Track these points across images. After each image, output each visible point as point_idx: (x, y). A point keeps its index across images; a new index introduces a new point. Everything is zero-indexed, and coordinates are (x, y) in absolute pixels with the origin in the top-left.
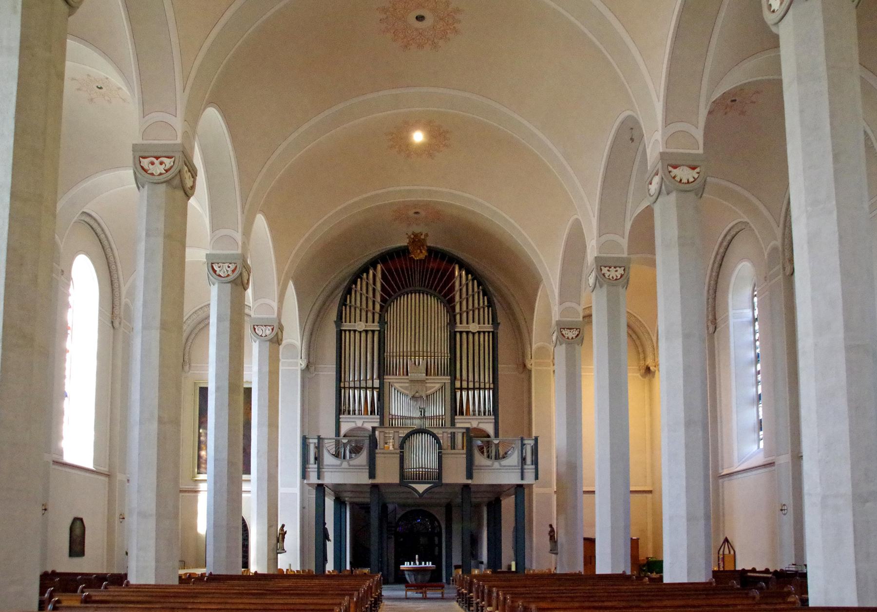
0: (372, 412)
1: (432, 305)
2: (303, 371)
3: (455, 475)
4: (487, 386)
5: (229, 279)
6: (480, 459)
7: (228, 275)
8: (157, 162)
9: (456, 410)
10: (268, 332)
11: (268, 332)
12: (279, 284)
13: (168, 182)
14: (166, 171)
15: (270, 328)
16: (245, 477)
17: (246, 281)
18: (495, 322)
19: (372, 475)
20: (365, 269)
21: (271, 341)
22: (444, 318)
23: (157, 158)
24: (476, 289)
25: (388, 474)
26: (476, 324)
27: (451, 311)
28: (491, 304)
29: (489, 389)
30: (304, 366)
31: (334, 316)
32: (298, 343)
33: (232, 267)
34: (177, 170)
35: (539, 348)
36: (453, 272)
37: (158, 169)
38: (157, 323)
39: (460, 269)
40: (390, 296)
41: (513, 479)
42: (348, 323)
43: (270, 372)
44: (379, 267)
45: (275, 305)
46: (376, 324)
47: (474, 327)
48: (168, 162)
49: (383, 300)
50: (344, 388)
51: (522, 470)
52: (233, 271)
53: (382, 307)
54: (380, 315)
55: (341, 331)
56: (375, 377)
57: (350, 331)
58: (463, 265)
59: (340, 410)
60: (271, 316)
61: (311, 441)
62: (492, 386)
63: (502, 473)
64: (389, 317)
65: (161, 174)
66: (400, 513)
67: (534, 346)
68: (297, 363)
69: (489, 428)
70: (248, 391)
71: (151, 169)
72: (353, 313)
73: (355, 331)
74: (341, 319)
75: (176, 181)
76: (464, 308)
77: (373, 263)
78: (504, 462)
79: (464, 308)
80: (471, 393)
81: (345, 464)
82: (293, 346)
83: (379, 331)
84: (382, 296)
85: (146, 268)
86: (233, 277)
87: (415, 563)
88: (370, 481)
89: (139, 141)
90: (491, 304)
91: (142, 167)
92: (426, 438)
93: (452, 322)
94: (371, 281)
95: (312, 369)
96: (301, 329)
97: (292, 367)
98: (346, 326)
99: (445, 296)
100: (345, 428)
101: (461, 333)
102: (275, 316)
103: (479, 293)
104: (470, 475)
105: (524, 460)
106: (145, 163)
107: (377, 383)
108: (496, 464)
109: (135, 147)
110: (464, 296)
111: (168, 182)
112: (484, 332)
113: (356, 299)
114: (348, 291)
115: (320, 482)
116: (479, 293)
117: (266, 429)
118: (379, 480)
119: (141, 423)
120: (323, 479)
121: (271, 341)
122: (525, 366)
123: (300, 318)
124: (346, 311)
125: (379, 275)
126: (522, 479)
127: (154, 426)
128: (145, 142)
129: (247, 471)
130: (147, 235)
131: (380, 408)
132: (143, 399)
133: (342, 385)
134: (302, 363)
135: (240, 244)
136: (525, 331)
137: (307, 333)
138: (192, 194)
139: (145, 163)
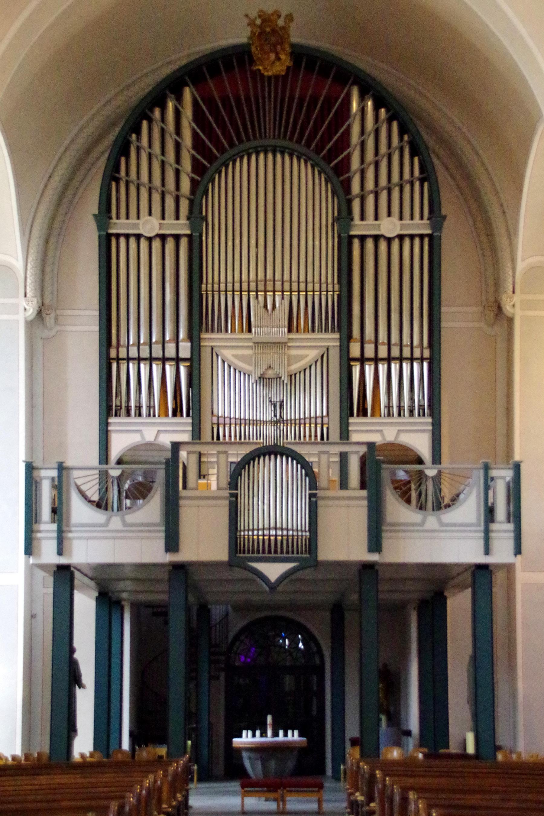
2: (30, 325)
3: (344, 541)
4: (417, 353)
9: (353, 404)
18: (435, 215)
19: (172, 543)
20: (156, 99)
22: (327, 207)
25: (205, 542)
28: (427, 175)
29: (422, 359)
30: (31, 312)
31: (92, 205)
32: (18, 264)
35: (532, 268)
40: (211, 158)
42: (123, 221)
44: (187, 94)
46: (183, 221)
47: (389, 227)
51: (487, 532)
53: (194, 184)
54: (192, 203)
55: (109, 236)
58: (369, 88)
59: (109, 408)
61: (44, 473)
62: (427, 354)
63: (440, 539)
64: (216, 202)
66: (238, 624)
67: (521, 266)
73: (138, 237)
74: (109, 210)
76: (370, 185)
77: (173, 86)
79: (370, 185)
81: (116, 522)
83: (190, 237)
88: (168, 558)
90: (427, 175)
93: (344, 217)
95: (50, 320)
99: (328, 158)
100: (119, 444)
101: (363, 238)
104: (375, 543)
107: (185, 350)
108: (432, 521)
110: (370, 156)
113: (140, 167)
114: (122, 149)
115: (63, 561)
118: (187, 554)
120: (70, 555)
125: (188, 112)
126: (487, 551)
131: (190, 402)
133: (113, 353)
134: (28, 307)
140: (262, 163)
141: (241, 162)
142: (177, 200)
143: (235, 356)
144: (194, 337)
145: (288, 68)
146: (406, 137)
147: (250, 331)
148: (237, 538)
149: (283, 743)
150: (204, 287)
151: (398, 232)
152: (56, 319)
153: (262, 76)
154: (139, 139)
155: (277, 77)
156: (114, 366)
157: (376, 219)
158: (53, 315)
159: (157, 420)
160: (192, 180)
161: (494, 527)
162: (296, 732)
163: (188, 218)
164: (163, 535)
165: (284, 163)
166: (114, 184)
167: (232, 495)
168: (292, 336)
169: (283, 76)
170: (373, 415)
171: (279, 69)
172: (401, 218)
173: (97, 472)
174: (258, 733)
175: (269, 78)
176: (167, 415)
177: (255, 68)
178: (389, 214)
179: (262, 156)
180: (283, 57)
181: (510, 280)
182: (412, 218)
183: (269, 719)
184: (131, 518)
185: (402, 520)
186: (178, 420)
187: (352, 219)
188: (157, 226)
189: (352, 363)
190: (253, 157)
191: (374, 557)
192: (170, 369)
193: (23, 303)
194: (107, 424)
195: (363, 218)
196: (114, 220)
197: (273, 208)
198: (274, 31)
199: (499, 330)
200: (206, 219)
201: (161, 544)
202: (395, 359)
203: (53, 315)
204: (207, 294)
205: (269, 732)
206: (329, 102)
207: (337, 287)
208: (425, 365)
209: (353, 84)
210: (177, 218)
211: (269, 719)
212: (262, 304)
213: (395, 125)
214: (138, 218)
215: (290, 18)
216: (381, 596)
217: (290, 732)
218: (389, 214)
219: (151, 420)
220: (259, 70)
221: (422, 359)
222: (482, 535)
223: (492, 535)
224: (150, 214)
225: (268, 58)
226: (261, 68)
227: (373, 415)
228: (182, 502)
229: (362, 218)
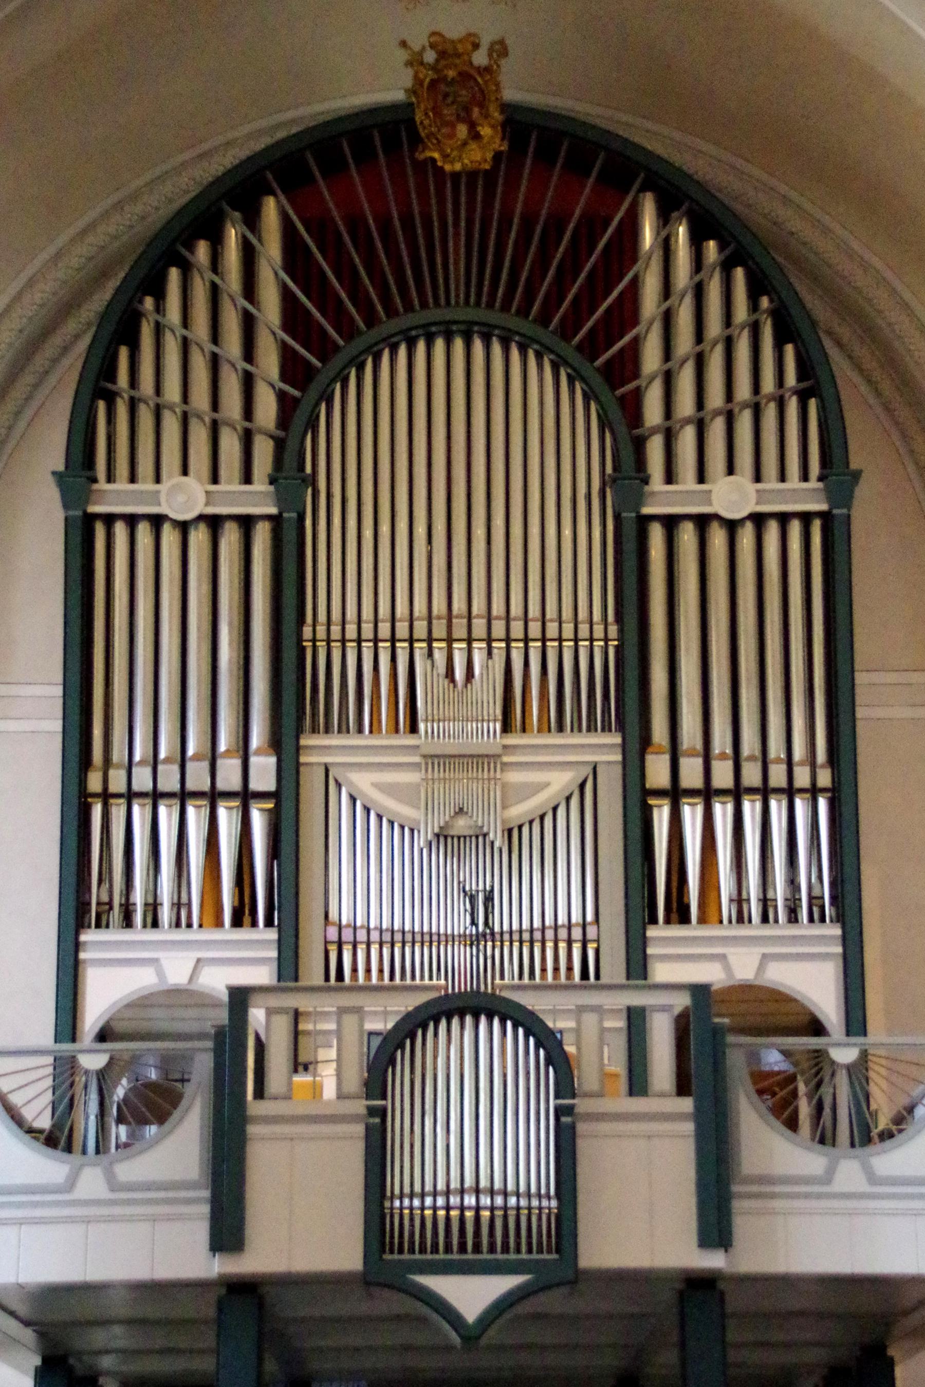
0: (242, 915)
3: (641, 1224)
4: (802, 778)
9: (655, 896)
18: (836, 470)
19: (227, 1232)
20: (200, 221)
22: (586, 457)
24: (741, 312)
25: (305, 1226)
31: (50, 449)
39: (664, 218)
46: (260, 485)
47: (732, 496)
49: (293, 369)
50: (106, 796)
54: (280, 445)
59: (82, 908)
62: (824, 779)
73: (157, 521)
74: (89, 462)
76: (685, 405)
77: (239, 192)
79: (685, 405)
81: (92, 1181)
83: (276, 520)
84: (288, 359)
90: (814, 383)
93: (626, 473)
98: (113, 496)
99: (590, 348)
100: (107, 990)
101: (671, 523)
103: (755, 330)
104: (716, 1228)
108: (849, 1172)
110: (684, 343)
113: (163, 368)
114: (121, 328)
116: (755, 330)
118: (261, 1258)
124: (112, 428)
125: (272, 249)
133: (94, 783)
140: (442, 363)
142: (247, 439)
144: (283, 743)
145: (498, 156)
146: (765, 302)
147: (413, 729)
148: (303, 649)
150: (307, 632)
154: (160, 308)
155: (472, 175)
157: (701, 479)
160: (282, 397)
163: (272, 481)
164: (206, 1209)
166: (101, 405)
168: (513, 740)
169: (486, 170)
171: (477, 157)
175: (456, 176)
177: (421, 156)
180: (486, 131)
182: (783, 478)
184: (133, 1169)
185: (779, 1169)
186: (244, 934)
187: (646, 481)
188: (202, 498)
189: (651, 802)
190: (421, 346)
191: (714, 1261)
195: (670, 477)
196: (102, 485)
198: (465, 77)
201: (201, 1232)
204: (315, 648)
206: (592, 225)
210: (247, 478)
213: (739, 274)
214: (158, 480)
215: (500, 49)
220: (433, 160)
225: (452, 136)
226: (436, 155)
227: (702, 920)
228: (253, 1130)
229: (670, 477)
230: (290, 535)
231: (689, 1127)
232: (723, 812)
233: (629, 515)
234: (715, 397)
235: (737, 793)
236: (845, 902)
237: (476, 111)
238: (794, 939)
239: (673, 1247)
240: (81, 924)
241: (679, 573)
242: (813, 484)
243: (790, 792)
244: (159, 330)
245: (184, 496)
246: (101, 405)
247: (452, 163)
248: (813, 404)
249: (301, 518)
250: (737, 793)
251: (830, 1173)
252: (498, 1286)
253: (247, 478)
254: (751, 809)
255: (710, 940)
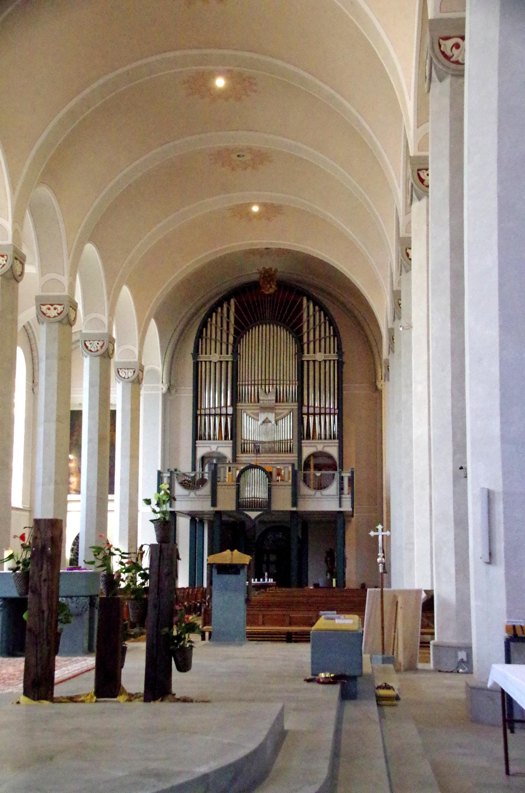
0: (226, 438)
1: (283, 337)
2: (164, 395)
3: (282, 503)
4: (332, 411)
5: (98, 353)
6: (304, 490)
7: (97, 350)
8: (52, 308)
9: (303, 433)
10: (130, 375)
11: (130, 375)
12: (139, 333)
13: (60, 322)
14: (59, 314)
15: (132, 371)
16: (110, 497)
17: (111, 352)
18: (340, 352)
19: (214, 503)
20: (219, 304)
21: (133, 382)
22: (292, 348)
23: (52, 305)
24: (323, 320)
25: (227, 503)
26: (322, 354)
27: (299, 340)
28: (336, 334)
29: (334, 414)
30: (165, 390)
31: (191, 348)
32: (159, 368)
33: (101, 343)
34: (66, 313)
36: (301, 304)
37: (53, 313)
38: (54, 417)
39: (308, 301)
40: (242, 328)
41: (332, 506)
42: (204, 355)
43: (132, 409)
44: (232, 301)
45: (136, 351)
46: (230, 355)
47: (320, 356)
48: (60, 308)
49: (236, 332)
50: (201, 415)
51: (340, 498)
52: (101, 347)
53: (235, 339)
54: (233, 347)
55: (198, 362)
56: (229, 404)
57: (206, 362)
58: (310, 298)
59: (197, 436)
60: (132, 360)
61: (165, 475)
62: (337, 411)
63: (325, 501)
64: (243, 348)
65: (55, 317)
68: (158, 387)
69: (334, 451)
70: (113, 413)
71: (49, 313)
72: (208, 345)
73: (210, 362)
74: (198, 352)
75: (65, 321)
76: (311, 338)
77: (226, 298)
78: (326, 492)
79: (311, 338)
80: (317, 418)
81: (192, 494)
82: (153, 371)
83: (233, 362)
84: (235, 329)
85: (46, 380)
86: (101, 351)
87: (264, 580)
88: (212, 509)
89: (39, 293)
90: (336, 334)
91: (443, 53)
92: (257, 471)
93: (300, 351)
94: (225, 315)
95: (173, 392)
96: (162, 354)
97: (153, 392)
98: (202, 357)
99: (293, 328)
100: (201, 452)
101: (308, 361)
102: (136, 360)
103: (325, 323)
104: (295, 503)
105: (341, 489)
106: (44, 308)
107: (230, 411)
108: (318, 493)
109: (38, 298)
110: (311, 326)
111: (60, 322)
112: (330, 361)
113: (212, 331)
114: (204, 324)
115: (172, 510)
116: (325, 323)
117: (128, 461)
118: (220, 507)
119: (43, 484)
120: (174, 507)
121: (133, 382)
122: (376, 388)
123: (161, 347)
124: (202, 344)
125: (233, 309)
126: (340, 506)
127: (52, 487)
128: (43, 294)
129: (112, 492)
130: (47, 358)
131: (233, 433)
132: (45, 468)
133: (199, 412)
134: (163, 388)
135: (107, 324)
136: (375, 350)
137: (168, 359)
138: (74, 324)
139: (44, 308)
140: (265, 328)
141: (255, 329)
142: (227, 345)
143: (252, 413)
144: (234, 404)
145: (275, 291)
146: (327, 318)
147: (259, 402)
149: (267, 583)
151: (323, 358)
152: (176, 391)
153: (265, 294)
154: (211, 321)
156: (199, 418)
157: (314, 353)
158: (174, 390)
159: (218, 442)
160: (234, 337)
161: (343, 496)
162: (272, 579)
163: (232, 354)
164: (210, 499)
165: (274, 328)
166: (200, 339)
167: (237, 485)
168: (278, 404)
170: (313, 439)
171: (272, 291)
172: (325, 353)
173: (58, 691)
174: (256, 580)
176: (222, 439)
178: (320, 351)
179: (264, 326)
180: (273, 286)
181: (380, 374)
182: (330, 353)
183: (266, 574)
184: (199, 492)
186: (227, 442)
187: (303, 354)
188: (218, 357)
189: (304, 416)
190: (261, 327)
191: (294, 509)
192: (223, 419)
193: (161, 386)
194: (196, 443)
195: (308, 353)
196: (200, 355)
197: (269, 349)
198: (269, 276)
199: (376, 395)
200: (240, 354)
201: (209, 503)
202: (323, 414)
203: (174, 390)
205: (266, 580)
206: (294, 302)
207: (297, 382)
208: (336, 417)
209: (304, 296)
210: (227, 353)
211: (266, 574)
212: (264, 390)
213: (322, 312)
214: (211, 354)
216: (60, 599)
217: (270, 579)
218: (320, 351)
219: (215, 442)
221: (334, 414)
222: (338, 499)
223: (343, 499)
224: (216, 353)
227: (313, 439)
229: (308, 353)
230: (235, 364)
231: (291, 487)
232: (317, 418)
233: (299, 360)
234: (317, 337)
235: (320, 414)
236: (340, 437)
237: (271, 283)
238: (331, 443)
239: (289, 507)
240: (196, 439)
241: (310, 372)
242: (336, 354)
243: (330, 414)
244: (211, 325)
245: (215, 357)
246: (200, 339)
247: (268, 290)
248: (336, 338)
249: (237, 361)
250: (320, 414)
251: (315, 494)
252: (259, 513)
253: (227, 353)
254: (322, 417)
255: (314, 443)
